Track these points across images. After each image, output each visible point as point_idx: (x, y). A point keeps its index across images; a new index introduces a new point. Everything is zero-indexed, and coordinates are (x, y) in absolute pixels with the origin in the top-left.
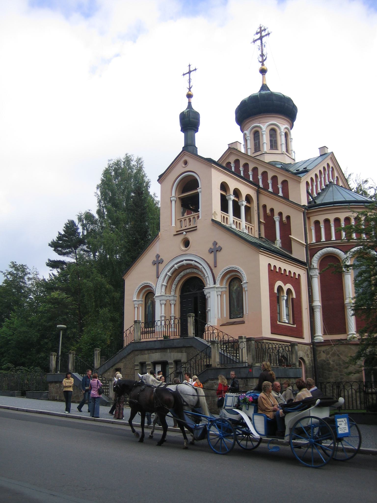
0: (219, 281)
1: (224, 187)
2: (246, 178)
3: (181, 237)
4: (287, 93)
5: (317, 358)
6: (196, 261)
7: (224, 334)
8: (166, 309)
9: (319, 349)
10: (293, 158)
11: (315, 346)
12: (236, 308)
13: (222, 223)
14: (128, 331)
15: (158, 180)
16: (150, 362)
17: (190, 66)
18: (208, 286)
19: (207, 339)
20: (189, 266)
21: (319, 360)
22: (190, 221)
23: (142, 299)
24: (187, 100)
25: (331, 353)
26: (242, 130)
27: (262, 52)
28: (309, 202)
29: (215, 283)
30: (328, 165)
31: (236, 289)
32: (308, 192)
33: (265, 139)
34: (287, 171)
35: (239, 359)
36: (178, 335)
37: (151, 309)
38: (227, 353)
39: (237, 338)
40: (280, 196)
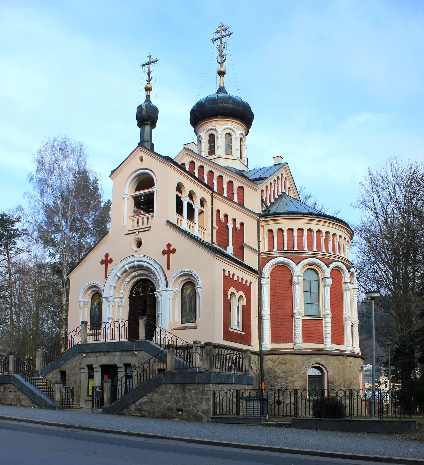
0: (172, 284)
1: (179, 187)
2: (200, 180)
3: (133, 236)
4: (245, 99)
5: (264, 366)
6: (148, 263)
7: (177, 338)
8: (116, 311)
9: (266, 357)
10: (246, 164)
11: (261, 354)
12: (189, 311)
13: (177, 225)
14: (74, 333)
15: (110, 176)
16: (97, 366)
17: (150, 56)
18: (161, 289)
19: (157, 342)
20: (141, 267)
21: (265, 367)
22: (138, 222)
23: (88, 298)
24: (145, 93)
25: (277, 361)
26: (196, 133)
27: (222, 52)
28: (263, 211)
29: (167, 287)
30: (282, 174)
31: (189, 294)
32: (262, 201)
33: (220, 142)
34: (244, 176)
35: (192, 364)
36: (125, 338)
37: (97, 310)
38: (180, 358)
39: (192, 343)
40: (234, 202)
